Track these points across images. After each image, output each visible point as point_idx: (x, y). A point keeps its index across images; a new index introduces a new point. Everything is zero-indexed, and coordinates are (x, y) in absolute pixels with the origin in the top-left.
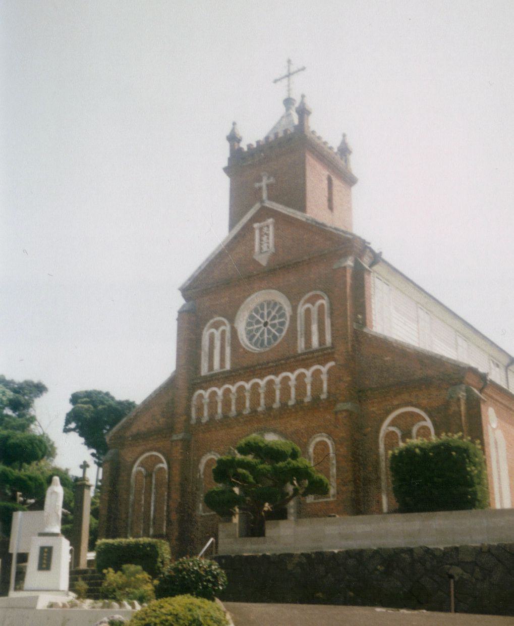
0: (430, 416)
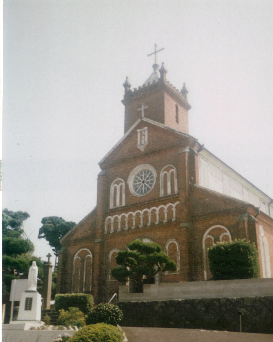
0: (229, 230)
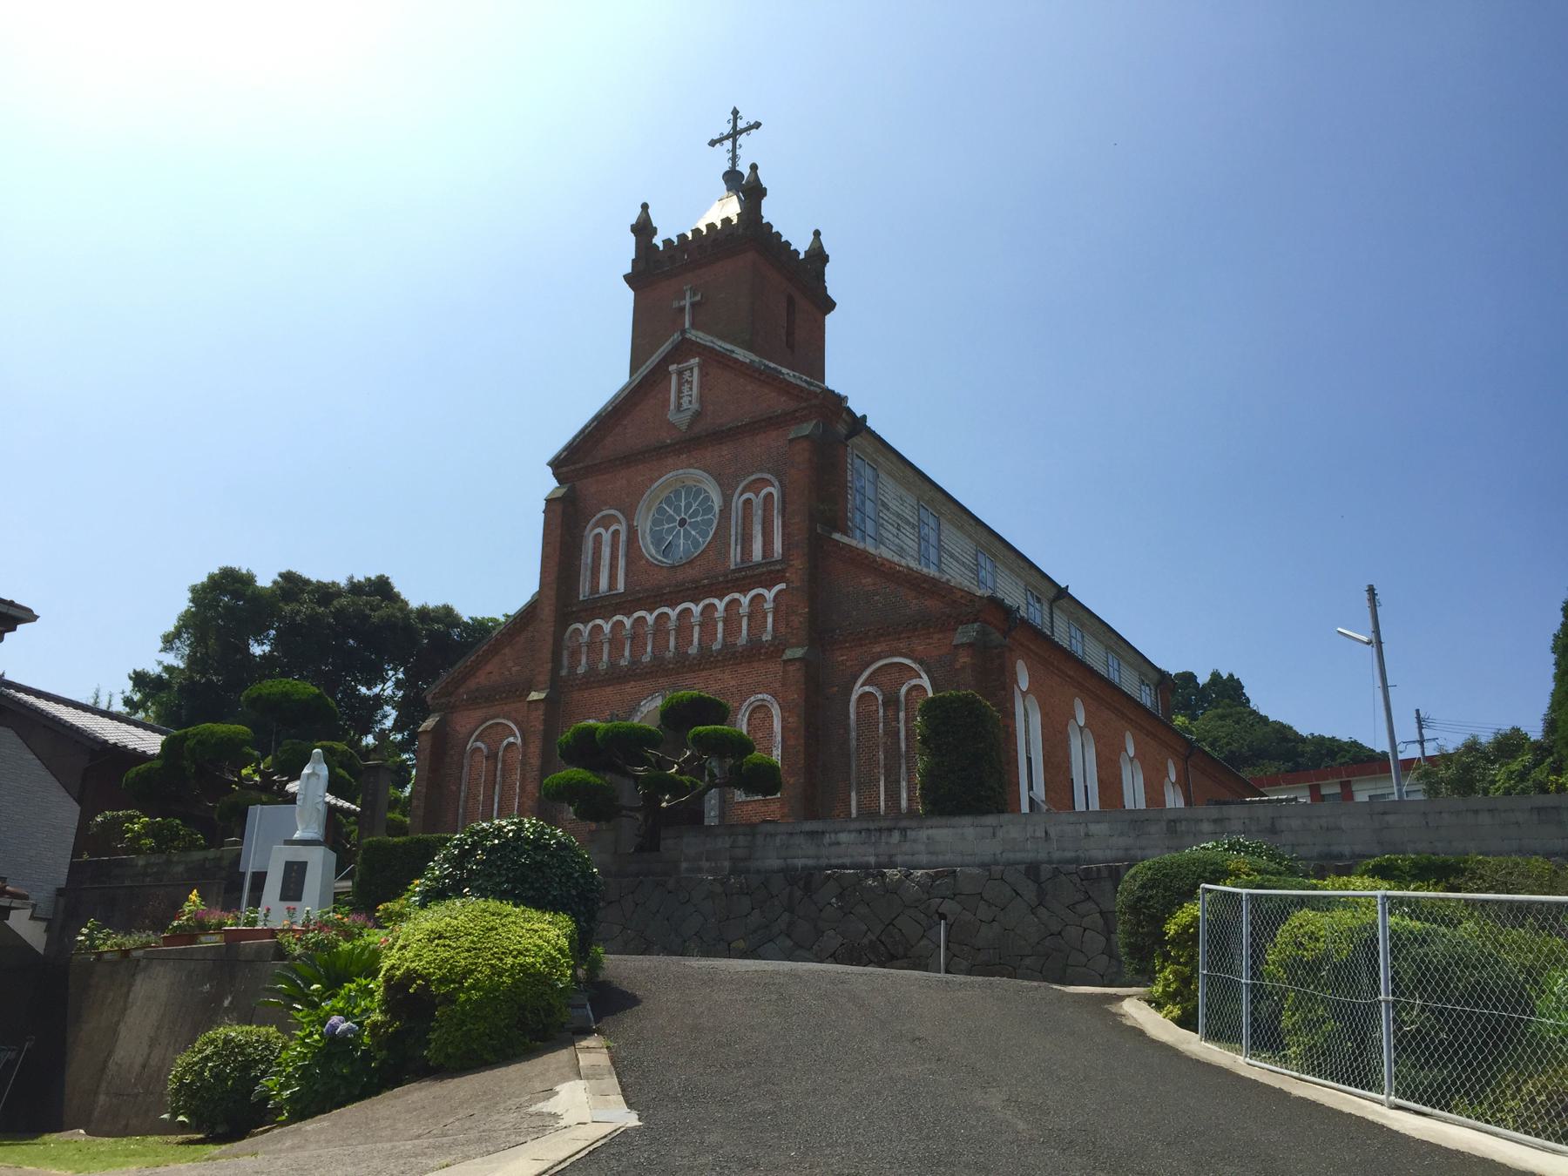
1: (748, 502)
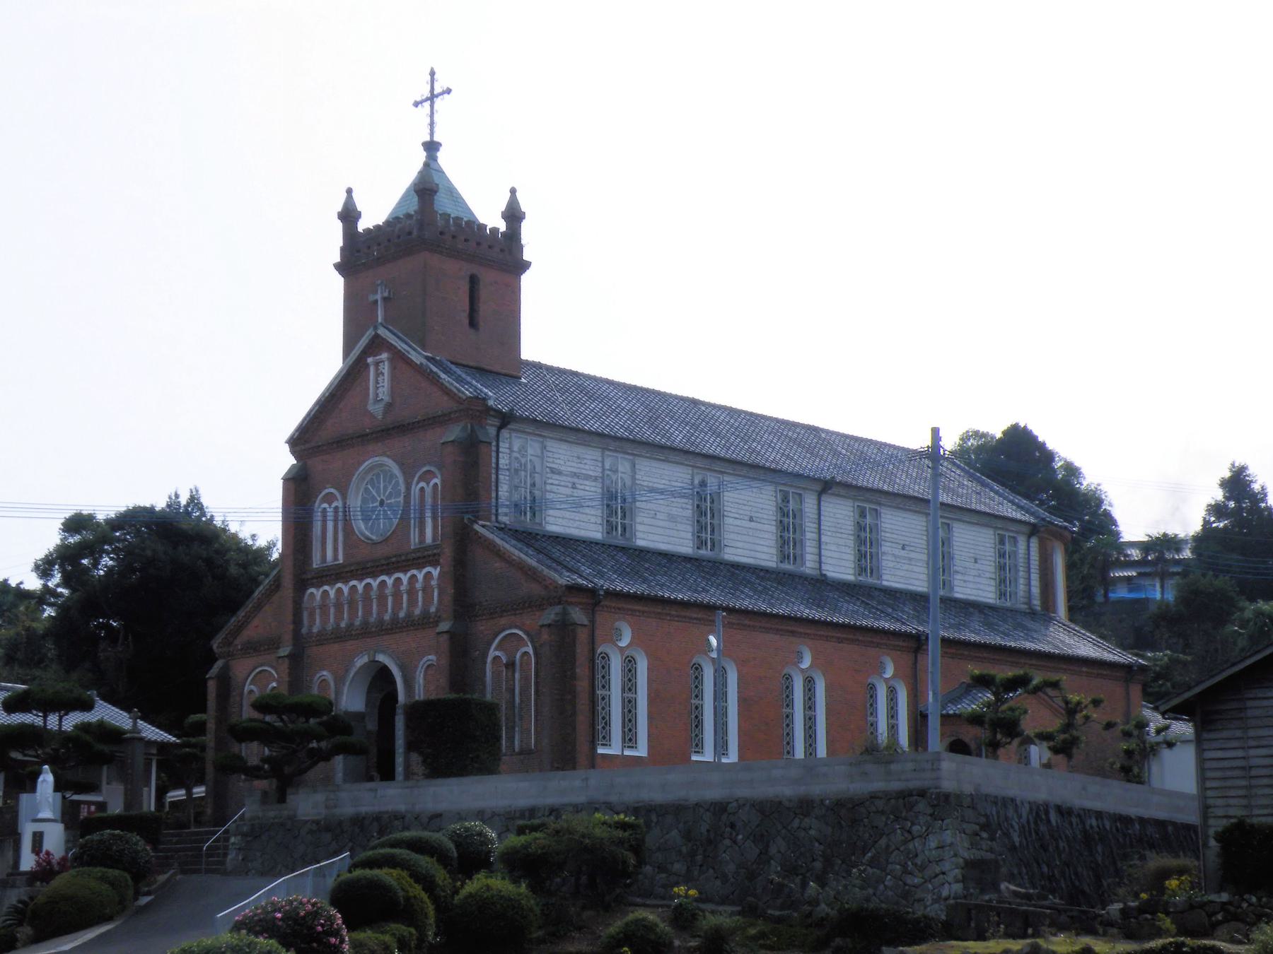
0: (532, 642)
1: (422, 489)
